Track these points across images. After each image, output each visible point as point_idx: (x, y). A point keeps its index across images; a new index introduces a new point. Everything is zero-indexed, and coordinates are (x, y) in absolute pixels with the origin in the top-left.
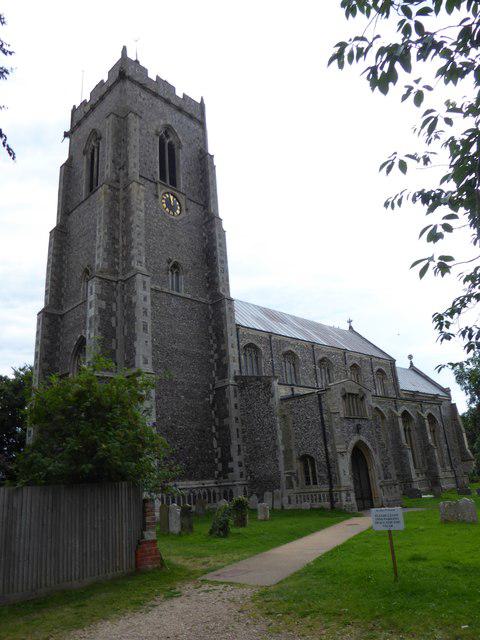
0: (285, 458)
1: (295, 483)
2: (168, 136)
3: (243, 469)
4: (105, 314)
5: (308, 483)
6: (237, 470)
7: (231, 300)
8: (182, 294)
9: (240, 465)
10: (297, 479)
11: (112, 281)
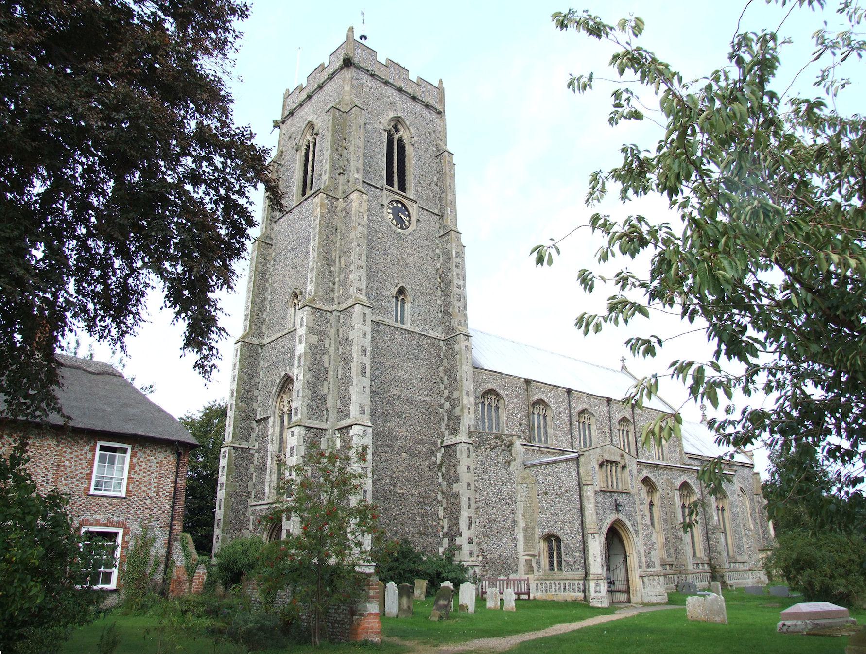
0: (525, 537)
1: (535, 567)
2: (397, 130)
3: (474, 548)
4: (316, 351)
5: (552, 568)
6: (466, 548)
7: (468, 336)
8: (407, 326)
9: (471, 542)
10: (538, 562)
11: (326, 311)
